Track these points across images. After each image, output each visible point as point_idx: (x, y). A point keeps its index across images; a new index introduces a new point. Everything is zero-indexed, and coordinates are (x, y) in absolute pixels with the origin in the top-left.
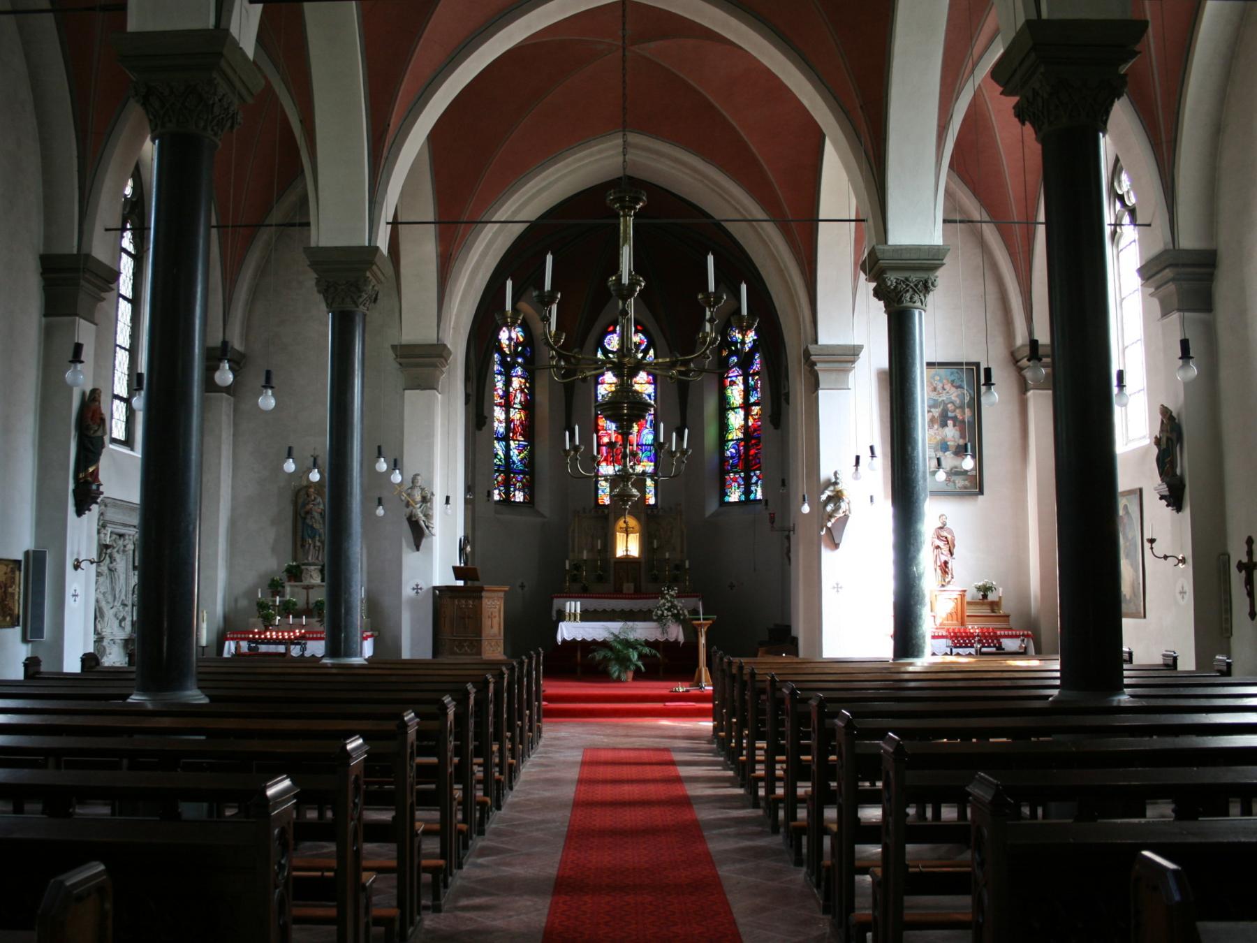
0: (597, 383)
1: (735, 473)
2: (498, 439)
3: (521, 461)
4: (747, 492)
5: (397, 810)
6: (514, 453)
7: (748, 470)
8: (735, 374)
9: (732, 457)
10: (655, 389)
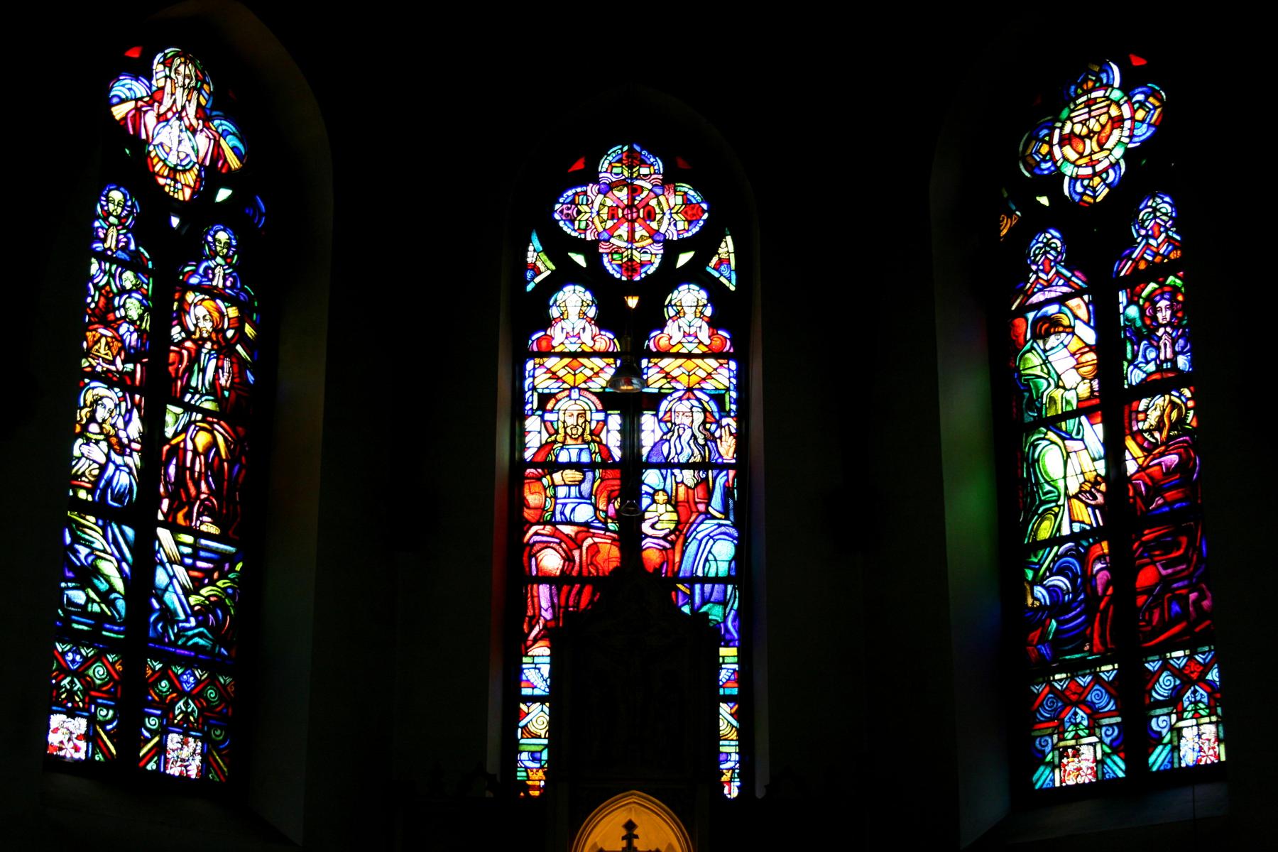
0: (521, 355)
1: (1074, 669)
2: (106, 515)
3: (201, 614)
4: (1135, 740)
5: (1147, 767)
6: (171, 581)
7: (1131, 648)
8: (1051, 283)
9: (1058, 604)
10: (742, 378)
